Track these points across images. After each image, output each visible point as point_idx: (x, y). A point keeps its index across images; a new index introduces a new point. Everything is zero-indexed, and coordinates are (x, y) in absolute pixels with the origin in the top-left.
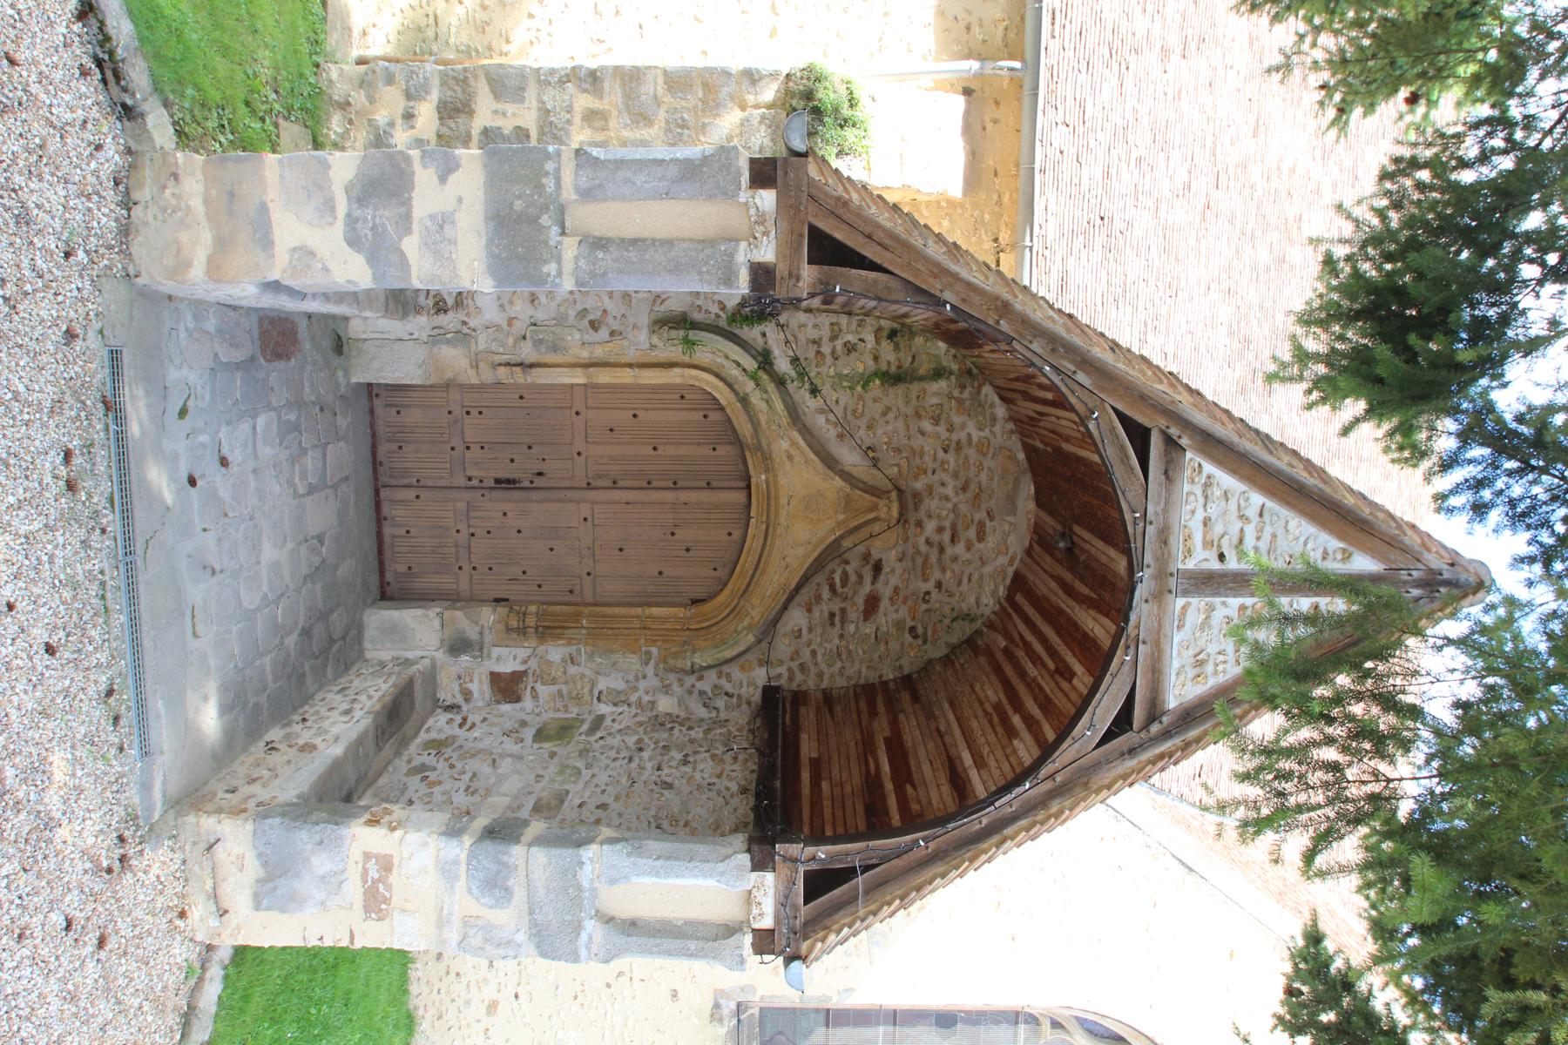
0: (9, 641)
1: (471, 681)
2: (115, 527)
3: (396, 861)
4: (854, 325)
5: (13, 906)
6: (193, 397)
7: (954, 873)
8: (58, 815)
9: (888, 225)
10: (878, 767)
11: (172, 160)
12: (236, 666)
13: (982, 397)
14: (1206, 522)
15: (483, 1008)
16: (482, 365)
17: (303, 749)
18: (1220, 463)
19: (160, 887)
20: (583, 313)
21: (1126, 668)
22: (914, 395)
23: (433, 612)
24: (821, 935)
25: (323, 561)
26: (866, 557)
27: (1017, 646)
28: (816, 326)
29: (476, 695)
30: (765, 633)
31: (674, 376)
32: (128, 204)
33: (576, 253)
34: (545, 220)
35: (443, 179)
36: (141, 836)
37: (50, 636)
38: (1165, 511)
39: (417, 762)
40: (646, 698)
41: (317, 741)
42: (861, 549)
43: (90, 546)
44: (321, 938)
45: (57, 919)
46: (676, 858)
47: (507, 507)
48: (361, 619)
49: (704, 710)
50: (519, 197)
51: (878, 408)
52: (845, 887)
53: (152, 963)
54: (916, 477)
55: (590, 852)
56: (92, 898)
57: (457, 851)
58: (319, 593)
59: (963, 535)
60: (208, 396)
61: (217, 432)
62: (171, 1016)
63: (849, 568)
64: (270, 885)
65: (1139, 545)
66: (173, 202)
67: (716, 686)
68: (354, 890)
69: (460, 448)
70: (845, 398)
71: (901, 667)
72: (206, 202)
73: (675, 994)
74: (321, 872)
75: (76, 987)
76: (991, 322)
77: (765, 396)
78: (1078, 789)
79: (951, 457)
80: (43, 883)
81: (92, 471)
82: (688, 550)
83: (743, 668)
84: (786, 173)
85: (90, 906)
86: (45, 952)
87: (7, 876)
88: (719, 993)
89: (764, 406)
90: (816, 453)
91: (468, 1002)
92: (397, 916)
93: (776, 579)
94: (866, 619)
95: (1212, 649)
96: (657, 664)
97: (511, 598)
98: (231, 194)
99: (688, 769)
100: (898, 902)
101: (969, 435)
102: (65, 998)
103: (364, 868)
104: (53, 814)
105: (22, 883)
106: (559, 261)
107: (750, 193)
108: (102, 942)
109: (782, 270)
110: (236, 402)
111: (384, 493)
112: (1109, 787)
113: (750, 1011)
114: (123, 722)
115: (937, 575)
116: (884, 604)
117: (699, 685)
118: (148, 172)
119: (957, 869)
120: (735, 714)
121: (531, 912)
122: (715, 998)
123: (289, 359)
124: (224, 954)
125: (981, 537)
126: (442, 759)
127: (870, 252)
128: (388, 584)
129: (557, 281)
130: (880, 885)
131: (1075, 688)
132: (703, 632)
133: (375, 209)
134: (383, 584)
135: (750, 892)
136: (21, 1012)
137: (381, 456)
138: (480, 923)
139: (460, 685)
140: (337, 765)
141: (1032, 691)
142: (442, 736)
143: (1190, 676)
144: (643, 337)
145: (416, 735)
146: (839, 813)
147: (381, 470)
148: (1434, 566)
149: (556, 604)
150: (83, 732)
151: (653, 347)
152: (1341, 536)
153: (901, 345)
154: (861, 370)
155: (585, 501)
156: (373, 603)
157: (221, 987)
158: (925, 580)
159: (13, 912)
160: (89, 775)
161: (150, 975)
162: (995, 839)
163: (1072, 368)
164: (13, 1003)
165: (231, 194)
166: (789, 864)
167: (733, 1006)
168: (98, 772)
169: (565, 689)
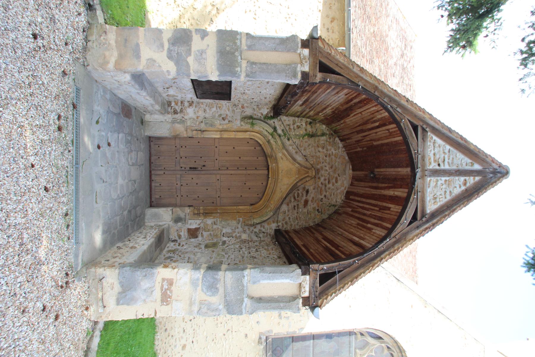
0: (31, 180)
1: (181, 232)
2: (73, 152)
3: (174, 281)
4: (299, 120)
5: (22, 297)
6: (101, 118)
7: (367, 271)
8: (43, 259)
9: (343, 61)
10: (325, 244)
11: (105, 27)
12: (108, 217)
13: (335, 141)
14: (434, 154)
15: (181, 347)
16: (188, 130)
17: (132, 248)
18: (437, 136)
19: (80, 297)
20: (220, 115)
21: (415, 200)
22: (317, 141)
23: (169, 209)
24: (325, 297)
25: (135, 189)
26: (304, 188)
27: (357, 208)
28: (289, 120)
29: (183, 236)
30: (276, 212)
31: (247, 135)
32: (86, 40)
33: (246, 65)
34: (237, 54)
35: (203, 38)
36: (74, 275)
37: (47, 184)
38: (423, 150)
39: (167, 256)
40: (238, 235)
41: (136, 246)
42: (303, 186)
43: (64, 156)
44: (143, 315)
45: (40, 305)
46: (276, 273)
47: (193, 176)
48: (145, 212)
49: (256, 238)
50: (228, 46)
51: (307, 144)
52: (332, 279)
53: (75, 328)
54: (318, 164)
55: (246, 272)
56: (54, 298)
57: (199, 275)
58: (134, 200)
59: (331, 181)
60: (105, 120)
61: (108, 134)
62: (80, 352)
63: (299, 192)
64: (124, 294)
65: (417, 161)
66: (104, 41)
67: (260, 230)
68: (157, 294)
69: (179, 158)
70: (297, 141)
71: (315, 222)
72: (116, 42)
73: (246, 335)
74: (145, 287)
75: (45, 337)
76: (373, 92)
77: (275, 140)
78: (402, 241)
79: (327, 158)
80: (35, 288)
81: (67, 128)
82: (249, 189)
83: (268, 224)
84: (312, 44)
85: (53, 302)
86: (33, 320)
87: (20, 282)
88: (261, 334)
89: (274, 143)
90: (290, 156)
91: (175, 346)
92: (174, 303)
93: (279, 195)
94: (305, 207)
95: (438, 194)
96: (242, 224)
97: (194, 205)
98: (126, 40)
99: (259, 253)
100: (350, 283)
101: (332, 152)
102: (40, 342)
103: (162, 284)
104: (42, 258)
105: (26, 286)
106: (241, 67)
107: (301, 49)
108: (57, 317)
109: (311, 74)
110: (114, 126)
111: (153, 172)
112: (412, 239)
113: (270, 340)
114: (70, 228)
115: (324, 193)
116: (310, 203)
117: (255, 230)
118: (95, 30)
119: (368, 270)
120: (266, 239)
121: (225, 296)
122: (260, 335)
123: (129, 119)
124: (101, 326)
125: (336, 182)
126: (176, 254)
127: (337, 69)
128: (153, 202)
129: (240, 73)
130: (344, 277)
131: (392, 211)
132: (256, 213)
133: (178, 47)
134: (151, 202)
135: (300, 284)
136: (21, 348)
137: (152, 160)
138: (206, 302)
139: (177, 233)
140: (144, 253)
141: (372, 217)
142: (173, 249)
143: (433, 202)
144: (238, 123)
145: (164, 248)
146: (322, 256)
147: (152, 165)
148: (495, 167)
149: (209, 206)
150: (56, 227)
151: (241, 125)
152: (471, 159)
153: (313, 126)
154: (302, 133)
155: (218, 174)
156: (148, 208)
157: (99, 339)
158: (321, 195)
159: (21, 300)
160: (57, 246)
161: (74, 334)
162: (379, 259)
163: (396, 107)
164: (17, 343)
165: (126, 40)
166: (315, 272)
167: (265, 338)
168: (60, 245)
169: (212, 233)
